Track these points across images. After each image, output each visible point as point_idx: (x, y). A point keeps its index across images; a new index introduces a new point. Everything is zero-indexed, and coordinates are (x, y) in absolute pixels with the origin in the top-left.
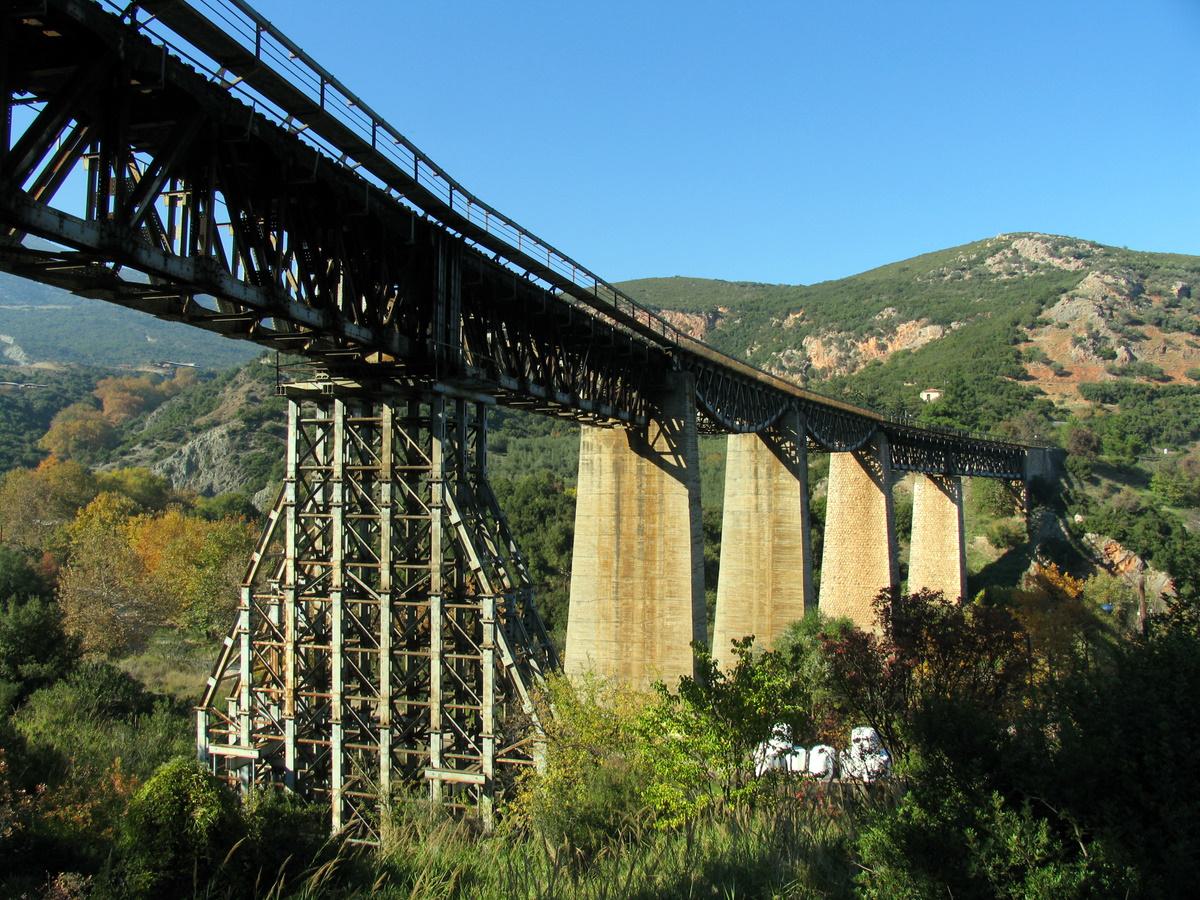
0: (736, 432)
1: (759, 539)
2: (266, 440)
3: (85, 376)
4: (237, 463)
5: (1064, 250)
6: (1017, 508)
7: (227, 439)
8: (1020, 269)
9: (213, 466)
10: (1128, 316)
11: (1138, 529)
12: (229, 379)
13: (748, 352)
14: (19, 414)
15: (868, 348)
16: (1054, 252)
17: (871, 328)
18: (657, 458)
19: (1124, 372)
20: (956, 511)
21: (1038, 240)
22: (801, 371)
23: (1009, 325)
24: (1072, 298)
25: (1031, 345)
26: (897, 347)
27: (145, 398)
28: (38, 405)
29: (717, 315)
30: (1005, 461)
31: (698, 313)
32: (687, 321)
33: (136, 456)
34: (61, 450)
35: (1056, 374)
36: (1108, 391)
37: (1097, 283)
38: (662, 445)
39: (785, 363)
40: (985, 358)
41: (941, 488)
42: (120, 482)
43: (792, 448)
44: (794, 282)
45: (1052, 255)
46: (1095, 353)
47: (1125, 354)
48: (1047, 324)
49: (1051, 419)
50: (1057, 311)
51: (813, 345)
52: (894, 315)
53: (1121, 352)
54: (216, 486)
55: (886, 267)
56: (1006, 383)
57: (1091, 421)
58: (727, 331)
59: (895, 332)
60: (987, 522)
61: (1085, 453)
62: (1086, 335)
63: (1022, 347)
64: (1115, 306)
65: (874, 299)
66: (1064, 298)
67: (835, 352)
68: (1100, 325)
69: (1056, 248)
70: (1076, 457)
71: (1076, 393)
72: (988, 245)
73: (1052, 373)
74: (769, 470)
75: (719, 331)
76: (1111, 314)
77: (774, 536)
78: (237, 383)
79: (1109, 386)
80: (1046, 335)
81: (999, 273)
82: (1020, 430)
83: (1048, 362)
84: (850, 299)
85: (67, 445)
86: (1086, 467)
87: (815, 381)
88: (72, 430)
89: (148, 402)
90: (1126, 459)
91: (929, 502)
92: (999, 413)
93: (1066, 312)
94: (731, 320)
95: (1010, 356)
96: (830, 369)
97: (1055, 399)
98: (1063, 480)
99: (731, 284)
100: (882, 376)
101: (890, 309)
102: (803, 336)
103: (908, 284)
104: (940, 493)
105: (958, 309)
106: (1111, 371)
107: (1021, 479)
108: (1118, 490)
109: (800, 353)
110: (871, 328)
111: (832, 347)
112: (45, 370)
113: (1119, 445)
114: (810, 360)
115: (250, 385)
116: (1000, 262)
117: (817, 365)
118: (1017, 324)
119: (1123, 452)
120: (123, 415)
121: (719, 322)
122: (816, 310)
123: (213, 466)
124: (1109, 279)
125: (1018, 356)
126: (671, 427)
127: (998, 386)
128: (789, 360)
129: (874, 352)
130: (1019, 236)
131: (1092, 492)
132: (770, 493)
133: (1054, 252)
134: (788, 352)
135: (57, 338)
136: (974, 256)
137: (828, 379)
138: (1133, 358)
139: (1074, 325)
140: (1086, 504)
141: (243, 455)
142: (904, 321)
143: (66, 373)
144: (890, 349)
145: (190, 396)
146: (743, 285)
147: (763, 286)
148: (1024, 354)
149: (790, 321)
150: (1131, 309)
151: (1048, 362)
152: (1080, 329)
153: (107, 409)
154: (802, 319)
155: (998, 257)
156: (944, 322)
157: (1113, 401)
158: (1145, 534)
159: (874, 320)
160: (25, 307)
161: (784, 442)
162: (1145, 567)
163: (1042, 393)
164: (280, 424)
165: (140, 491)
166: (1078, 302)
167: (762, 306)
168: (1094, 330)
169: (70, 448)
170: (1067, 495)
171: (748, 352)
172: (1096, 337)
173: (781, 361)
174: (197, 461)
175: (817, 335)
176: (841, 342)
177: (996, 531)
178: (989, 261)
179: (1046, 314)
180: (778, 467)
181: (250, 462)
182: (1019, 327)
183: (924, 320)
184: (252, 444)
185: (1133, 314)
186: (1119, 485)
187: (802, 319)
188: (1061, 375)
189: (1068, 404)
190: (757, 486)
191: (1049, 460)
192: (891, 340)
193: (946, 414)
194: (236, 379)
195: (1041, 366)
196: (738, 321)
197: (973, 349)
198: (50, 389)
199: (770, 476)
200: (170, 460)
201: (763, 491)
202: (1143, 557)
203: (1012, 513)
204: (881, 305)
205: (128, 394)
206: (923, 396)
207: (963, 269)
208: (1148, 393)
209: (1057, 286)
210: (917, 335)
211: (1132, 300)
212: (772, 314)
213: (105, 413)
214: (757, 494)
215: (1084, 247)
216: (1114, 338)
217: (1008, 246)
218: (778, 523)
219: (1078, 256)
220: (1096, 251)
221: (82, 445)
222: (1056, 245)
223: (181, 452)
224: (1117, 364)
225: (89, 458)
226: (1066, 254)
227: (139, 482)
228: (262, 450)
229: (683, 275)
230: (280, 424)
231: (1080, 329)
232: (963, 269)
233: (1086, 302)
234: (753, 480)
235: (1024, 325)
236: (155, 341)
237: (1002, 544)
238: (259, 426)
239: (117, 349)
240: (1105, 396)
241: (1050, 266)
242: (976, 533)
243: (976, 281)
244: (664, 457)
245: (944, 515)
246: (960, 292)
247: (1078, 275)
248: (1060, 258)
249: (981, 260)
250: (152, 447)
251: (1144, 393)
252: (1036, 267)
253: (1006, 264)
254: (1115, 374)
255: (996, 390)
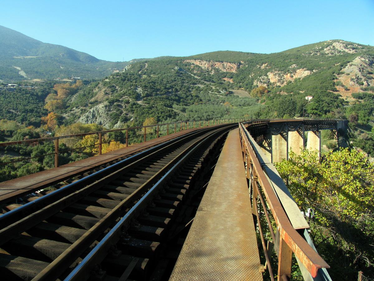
0: (274, 135)
1: (276, 156)
2: (116, 108)
3: (49, 83)
4: (108, 115)
5: (349, 46)
6: (334, 137)
7: (104, 108)
8: (335, 52)
9: (101, 116)
10: (368, 71)
11: (367, 146)
12: (96, 86)
13: (250, 76)
14: (35, 97)
15: (287, 77)
16: (346, 47)
17: (288, 71)
18: (265, 148)
19: (365, 89)
20: (319, 140)
21: (341, 43)
22: (267, 83)
23: (331, 74)
24: (351, 65)
25: (338, 80)
26: (296, 77)
27: (70, 90)
28: (40, 94)
29: (240, 64)
30: (331, 125)
31: (235, 63)
32: (231, 66)
33: (75, 111)
34: (51, 109)
35: (345, 90)
36: (360, 96)
37: (359, 60)
38: (266, 145)
39: (262, 80)
40: (324, 84)
41: (316, 134)
42: (89, 128)
43: (286, 135)
44: (263, 53)
45: (345, 48)
46: (357, 83)
47: (366, 84)
48: (343, 73)
49: (343, 105)
50: (346, 69)
51: (270, 75)
52: (296, 66)
53: (365, 83)
54: (102, 122)
55: (293, 49)
56: (330, 93)
57: (355, 105)
58: (244, 69)
59: (296, 72)
60: (326, 141)
61: (354, 121)
62: (355, 78)
63: (335, 81)
64: (364, 68)
65: (289, 60)
66: (348, 64)
67: (277, 78)
68: (359, 74)
69: (346, 46)
70: (351, 123)
71: (351, 96)
72: (325, 44)
73: (344, 90)
74: (279, 139)
75: (241, 69)
76: (363, 70)
77: (280, 155)
78: (99, 87)
79: (361, 94)
80: (342, 77)
81: (328, 54)
82: (335, 115)
83: (343, 86)
84: (282, 60)
85: (53, 108)
86: (354, 126)
87: (271, 86)
88: (54, 103)
89: (72, 92)
90: (365, 122)
91: (312, 138)
92: (329, 104)
93: (349, 70)
94: (245, 65)
95: (331, 84)
96: (276, 83)
97: (344, 98)
98: (348, 129)
99: (244, 53)
100: (293, 88)
101: (294, 65)
102: (267, 72)
103: (300, 56)
104: (315, 135)
105: (315, 66)
106: (362, 89)
107: (336, 129)
108: (363, 132)
109: (266, 77)
110: (288, 71)
111: (277, 76)
112: (38, 82)
113: (363, 119)
114: (269, 79)
115: (105, 89)
116: (329, 50)
117: (272, 81)
118: (334, 73)
119: (364, 120)
120: (64, 96)
121: (241, 66)
122: (271, 63)
123: (101, 116)
124: (363, 59)
125: (334, 84)
126: (268, 141)
127: (328, 94)
128: (263, 79)
129: (289, 78)
130: (335, 41)
131: (356, 133)
132: (279, 145)
133: (346, 47)
134: (263, 77)
135: (33, 68)
136: (321, 47)
137: (275, 86)
138: (369, 85)
139: (351, 74)
140: (354, 137)
141: (110, 113)
142: (299, 69)
143: (44, 82)
144: (294, 77)
145: (85, 91)
146: (248, 53)
147: (254, 54)
148: (336, 83)
149: (263, 66)
150: (369, 69)
151: (343, 86)
152: (353, 76)
153: (59, 95)
154: (267, 66)
155: (328, 48)
156: (311, 70)
157: (362, 99)
158: (369, 147)
159: (290, 68)
160: (21, 57)
161: (284, 133)
162: (369, 156)
163: (341, 96)
164: (119, 103)
165: (95, 130)
166: (353, 67)
167: (254, 61)
168: (357, 76)
169: (54, 109)
170: (349, 134)
171: (250, 76)
172: (357, 78)
173: (261, 80)
174: (95, 114)
175: (272, 72)
176: (279, 74)
177: (329, 144)
178: (325, 49)
179: (343, 70)
180: (281, 139)
181: (112, 115)
182: (335, 74)
183: (305, 69)
184: (112, 110)
185: (370, 71)
186: (363, 130)
187: (267, 66)
188: (347, 90)
189: (348, 100)
190: (276, 143)
191: (343, 124)
192: (295, 75)
193: (315, 109)
194: (98, 86)
195: (341, 87)
196: (247, 66)
197: (321, 81)
198: (42, 89)
199: (279, 141)
200: (87, 114)
201: (278, 144)
202: (368, 154)
203: (333, 139)
204: (291, 63)
205: (65, 90)
206: (306, 98)
207: (317, 52)
208: (372, 96)
209: (345, 59)
210: (303, 73)
211: (370, 66)
212: (257, 64)
213: (59, 96)
214: (276, 145)
215: (355, 46)
216: (363, 79)
217: (331, 45)
218: (281, 152)
219: (353, 49)
220: (359, 47)
221: (57, 108)
222: (347, 45)
223: (90, 112)
224: (364, 87)
225: (60, 112)
226: (350, 48)
227: (95, 128)
228: (115, 111)
229: (230, 50)
230: (119, 103)
231: (353, 76)
232: (317, 52)
233: (355, 67)
234: (275, 142)
235: (336, 74)
236: (63, 68)
237: (330, 148)
238: (113, 104)
239: (52, 71)
240: (360, 97)
241: (344, 52)
242: (323, 144)
243: (321, 56)
244: (266, 148)
245: (316, 141)
246: (316, 60)
247: (353, 56)
248: (348, 49)
249: (323, 49)
250: (79, 109)
251: (371, 96)
252: (340, 52)
253: (330, 51)
254: (363, 90)
255: (328, 95)
